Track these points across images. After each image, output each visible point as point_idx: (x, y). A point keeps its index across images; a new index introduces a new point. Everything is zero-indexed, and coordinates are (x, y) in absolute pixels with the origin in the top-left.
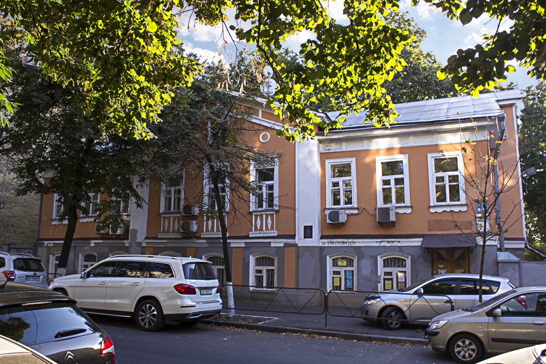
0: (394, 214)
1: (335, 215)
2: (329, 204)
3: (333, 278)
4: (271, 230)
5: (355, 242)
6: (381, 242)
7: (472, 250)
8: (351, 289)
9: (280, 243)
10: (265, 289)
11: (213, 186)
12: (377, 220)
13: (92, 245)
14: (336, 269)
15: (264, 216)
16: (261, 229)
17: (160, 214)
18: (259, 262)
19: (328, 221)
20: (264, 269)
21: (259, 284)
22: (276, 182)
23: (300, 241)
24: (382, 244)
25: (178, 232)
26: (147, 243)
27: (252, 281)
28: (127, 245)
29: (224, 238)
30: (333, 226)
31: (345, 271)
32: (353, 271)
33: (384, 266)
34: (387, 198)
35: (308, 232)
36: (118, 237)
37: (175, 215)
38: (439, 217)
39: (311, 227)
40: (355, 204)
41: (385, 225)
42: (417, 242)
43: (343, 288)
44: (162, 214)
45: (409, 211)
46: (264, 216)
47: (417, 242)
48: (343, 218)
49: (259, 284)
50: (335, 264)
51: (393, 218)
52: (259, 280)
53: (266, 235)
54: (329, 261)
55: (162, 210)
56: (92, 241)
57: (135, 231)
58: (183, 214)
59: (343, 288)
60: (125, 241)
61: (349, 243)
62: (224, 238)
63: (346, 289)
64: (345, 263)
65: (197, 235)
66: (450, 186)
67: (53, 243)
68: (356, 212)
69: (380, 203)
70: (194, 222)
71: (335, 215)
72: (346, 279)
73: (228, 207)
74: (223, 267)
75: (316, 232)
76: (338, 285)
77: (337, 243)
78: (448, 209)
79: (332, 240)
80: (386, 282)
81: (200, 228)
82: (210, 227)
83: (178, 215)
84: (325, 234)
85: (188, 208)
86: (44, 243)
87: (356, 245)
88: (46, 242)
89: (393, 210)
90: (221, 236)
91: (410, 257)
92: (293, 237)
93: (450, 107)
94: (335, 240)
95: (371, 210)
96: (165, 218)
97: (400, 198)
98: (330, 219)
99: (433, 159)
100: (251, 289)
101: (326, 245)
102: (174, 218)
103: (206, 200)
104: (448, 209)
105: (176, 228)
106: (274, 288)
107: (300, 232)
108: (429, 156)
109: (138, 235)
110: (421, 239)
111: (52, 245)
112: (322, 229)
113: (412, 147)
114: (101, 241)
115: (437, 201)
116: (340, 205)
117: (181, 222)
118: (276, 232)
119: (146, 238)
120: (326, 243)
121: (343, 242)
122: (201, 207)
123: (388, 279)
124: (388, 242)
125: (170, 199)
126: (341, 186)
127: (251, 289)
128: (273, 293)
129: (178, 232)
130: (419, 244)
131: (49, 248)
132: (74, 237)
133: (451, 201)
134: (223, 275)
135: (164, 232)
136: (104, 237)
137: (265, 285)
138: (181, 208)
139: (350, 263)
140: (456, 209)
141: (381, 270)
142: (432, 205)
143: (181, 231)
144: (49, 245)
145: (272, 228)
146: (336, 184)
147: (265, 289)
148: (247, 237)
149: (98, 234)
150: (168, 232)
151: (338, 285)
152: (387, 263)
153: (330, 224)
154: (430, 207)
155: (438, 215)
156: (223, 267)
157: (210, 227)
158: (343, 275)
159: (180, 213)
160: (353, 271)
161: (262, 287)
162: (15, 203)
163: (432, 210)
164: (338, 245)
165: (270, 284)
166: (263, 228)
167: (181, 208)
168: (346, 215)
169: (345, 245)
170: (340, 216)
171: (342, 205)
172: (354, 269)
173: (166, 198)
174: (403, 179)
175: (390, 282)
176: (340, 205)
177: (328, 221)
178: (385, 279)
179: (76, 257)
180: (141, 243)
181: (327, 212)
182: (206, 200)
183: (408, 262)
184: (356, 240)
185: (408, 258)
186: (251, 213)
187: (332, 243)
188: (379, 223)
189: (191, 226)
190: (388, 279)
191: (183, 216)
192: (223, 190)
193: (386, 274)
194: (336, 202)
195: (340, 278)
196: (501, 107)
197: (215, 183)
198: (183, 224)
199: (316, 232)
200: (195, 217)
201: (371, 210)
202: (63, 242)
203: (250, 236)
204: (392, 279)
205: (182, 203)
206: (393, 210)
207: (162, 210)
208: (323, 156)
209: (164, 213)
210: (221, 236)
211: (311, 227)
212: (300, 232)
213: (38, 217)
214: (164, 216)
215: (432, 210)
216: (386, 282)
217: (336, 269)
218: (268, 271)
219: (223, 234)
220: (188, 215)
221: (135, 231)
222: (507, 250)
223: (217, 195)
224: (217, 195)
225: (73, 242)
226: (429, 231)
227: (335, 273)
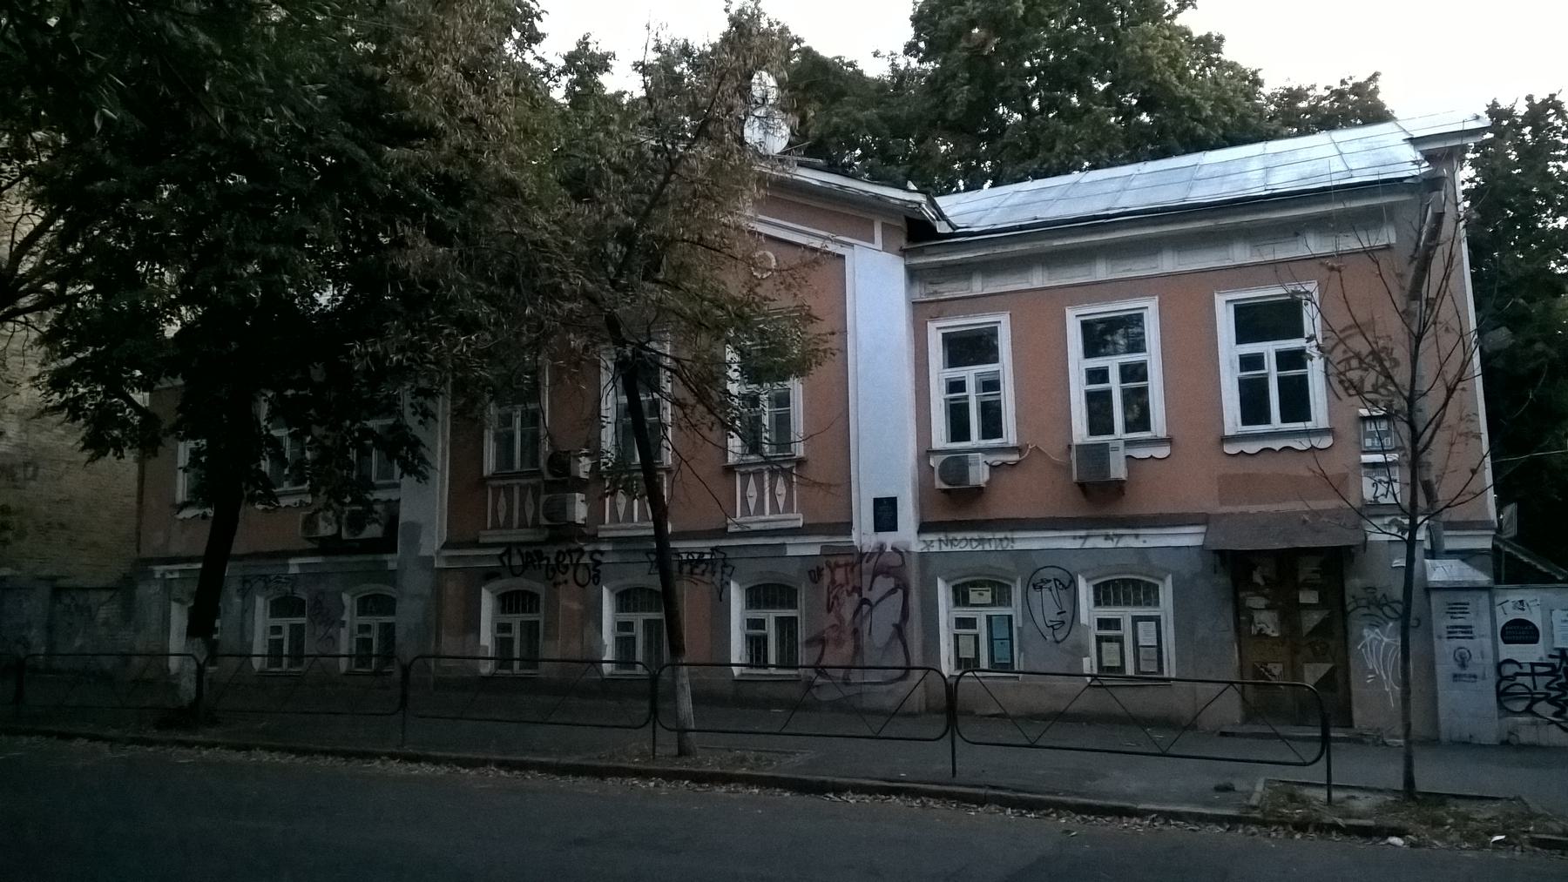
0: (1123, 461)
1: (956, 466)
2: (939, 437)
3: (957, 637)
4: (785, 511)
5: (1013, 540)
6: (1086, 537)
7: (1352, 556)
8: (1008, 667)
9: (809, 547)
10: (773, 671)
11: (624, 399)
12: (1075, 478)
13: (294, 570)
14: (965, 613)
15: (516, 489)
16: (509, 524)
17: (482, 482)
18: (755, 598)
19: (939, 484)
20: (770, 616)
21: (758, 659)
22: (1004, 366)
23: (864, 535)
24: (1089, 544)
25: (536, 524)
26: (449, 559)
27: (737, 650)
28: (392, 566)
29: (660, 534)
30: (953, 499)
31: (989, 618)
32: (1010, 617)
33: (1097, 603)
34: (1099, 417)
35: (885, 513)
36: (372, 546)
37: (524, 481)
38: (1251, 467)
39: (892, 502)
40: (1010, 435)
41: (1098, 496)
42: (1190, 537)
43: (984, 662)
44: (490, 478)
45: (1162, 452)
46: (516, 489)
47: (1190, 537)
48: (979, 474)
49: (758, 659)
50: (960, 597)
51: (1118, 470)
52: (756, 645)
53: (773, 526)
54: (943, 593)
55: (489, 465)
56: (292, 561)
57: (415, 528)
58: (548, 477)
59: (984, 662)
60: (388, 557)
61: (994, 542)
62: (660, 534)
63: (994, 666)
64: (987, 597)
65: (585, 531)
66: (1279, 379)
67: (181, 571)
68: (1015, 457)
69: (1080, 431)
70: (579, 496)
71: (956, 466)
72: (991, 640)
73: (668, 458)
74: (658, 615)
75: (907, 516)
76: (971, 655)
77: (964, 543)
78: (1277, 445)
79: (951, 536)
80: (1104, 645)
81: (596, 514)
82: (752, 504)
83: (532, 481)
84: (933, 518)
85: (561, 464)
86: (152, 572)
87: (1018, 546)
88: (159, 570)
89: (1117, 449)
90: (652, 532)
91: (1169, 580)
92: (847, 528)
93: (1272, 163)
94: (959, 536)
95: (1054, 450)
96: (496, 490)
97: (1296, 405)
98: (942, 478)
99: (1231, 308)
100: (736, 671)
101: (935, 549)
102: (523, 488)
103: (608, 437)
104: (1277, 445)
105: (530, 515)
106: (797, 668)
107: (864, 516)
108: (1220, 300)
109: (424, 540)
110: (1201, 529)
111: (176, 575)
112: (922, 504)
113: (1170, 275)
114: (319, 560)
115: (1245, 422)
116: (968, 439)
117: (543, 498)
118: (800, 516)
119: (445, 546)
120: (936, 543)
121: (981, 541)
122: (596, 453)
123: (1109, 639)
124: (1107, 537)
125: (512, 437)
126: (1115, 384)
127: (736, 671)
128: (796, 681)
129: (536, 524)
130: (1197, 541)
131: (167, 584)
132: (233, 552)
133: (1283, 421)
134: (659, 635)
135: (496, 526)
136: (328, 547)
137: (772, 660)
138: (543, 463)
139: (1001, 594)
140: (1301, 444)
141: (1088, 611)
142: (1229, 432)
143: (543, 521)
144: (169, 576)
145: (789, 507)
146: (1098, 375)
147: (773, 671)
148: (723, 533)
149: (309, 539)
150: (509, 524)
151: (971, 655)
152: (1103, 595)
153: (945, 491)
154: (1226, 440)
155: (1248, 460)
156: (658, 615)
157: (752, 504)
158: (982, 629)
159: (539, 473)
160: (1010, 617)
161: (766, 666)
162: (69, 463)
163: (1231, 449)
164: (968, 548)
165: (788, 658)
166: (764, 507)
167: (543, 463)
168: (987, 468)
169: (987, 547)
170: (971, 469)
171: (975, 439)
172: (1015, 610)
173: (497, 437)
174: (1143, 365)
175: (1116, 646)
176: (968, 439)
177: (939, 484)
178: (1099, 639)
179: (247, 610)
180: (431, 559)
181: (935, 462)
182: (608, 437)
183: (1166, 593)
184: (1017, 535)
185: (1162, 580)
186: (730, 470)
187: (952, 542)
188: (1082, 486)
189: (569, 508)
190: (1109, 639)
191: (548, 483)
192: (655, 407)
193: (1103, 623)
194: (959, 429)
195: (977, 637)
196: (1429, 157)
197: (631, 391)
198: (547, 504)
199: (907, 516)
200: (580, 485)
201: (1054, 450)
202: (200, 566)
203: (731, 529)
204: (1120, 640)
205: (546, 448)
206: (1117, 449)
207: (489, 465)
208: (921, 312)
209: (494, 476)
210: (652, 532)
211: (892, 502)
212: (864, 516)
213: (133, 501)
214: (495, 483)
215: (1231, 449)
216: (1104, 645)
217: (965, 613)
218: (779, 620)
219: (656, 528)
220: (561, 478)
221: (415, 528)
222: (1451, 554)
223: (640, 427)
224: (640, 427)
225: (229, 564)
226: (1222, 504)
227: (962, 623)
